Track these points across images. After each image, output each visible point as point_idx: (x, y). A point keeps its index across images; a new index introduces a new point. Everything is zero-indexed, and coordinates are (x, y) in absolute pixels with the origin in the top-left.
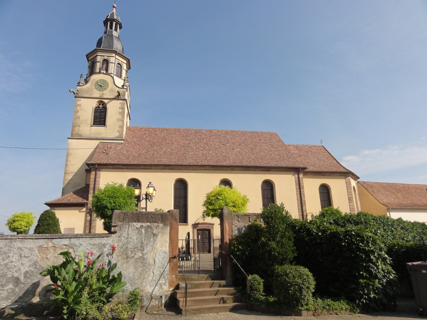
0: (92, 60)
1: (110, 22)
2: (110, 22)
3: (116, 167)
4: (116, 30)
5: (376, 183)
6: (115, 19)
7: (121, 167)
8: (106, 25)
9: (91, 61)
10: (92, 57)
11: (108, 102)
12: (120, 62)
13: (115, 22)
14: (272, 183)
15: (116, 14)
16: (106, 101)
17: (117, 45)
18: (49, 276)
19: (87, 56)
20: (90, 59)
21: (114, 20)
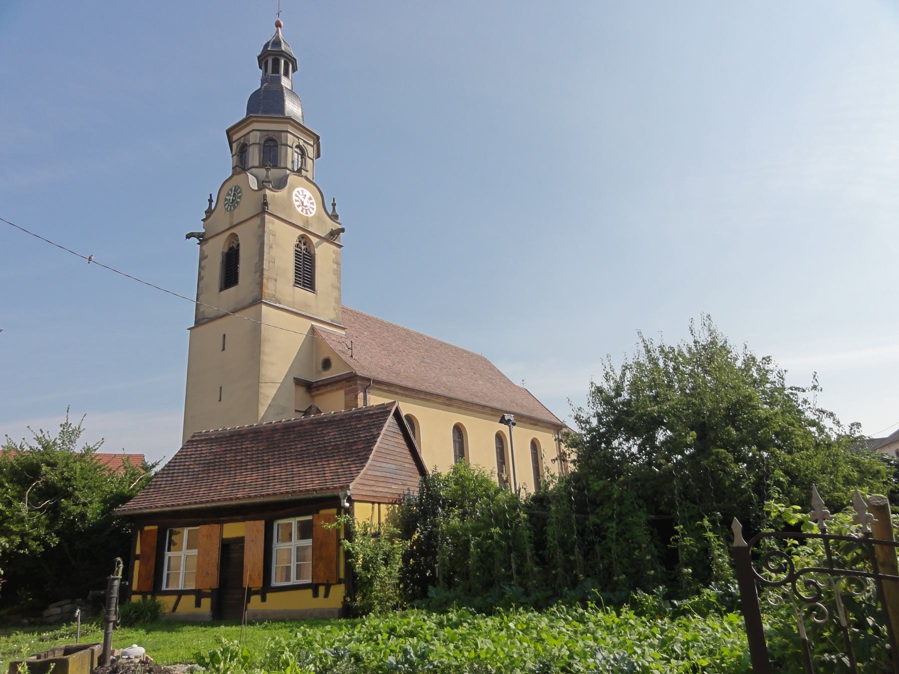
0: (242, 140)
1: (273, 57)
2: (273, 57)
3: (392, 389)
4: (286, 74)
5: (403, 329)
6: (283, 51)
7: (398, 391)
8: (263, 67)
9: (238, 142)
10: (238, 134)
11: (318, 244)
12: (302, 143)
13: (285, 57)
14: (414, 421)
15: (284, 41)
16: (314, 240)
17: (292, 107)
18: (263, 522)
19: (228, 132)
20: (235, 137)
21: (283, 54)
